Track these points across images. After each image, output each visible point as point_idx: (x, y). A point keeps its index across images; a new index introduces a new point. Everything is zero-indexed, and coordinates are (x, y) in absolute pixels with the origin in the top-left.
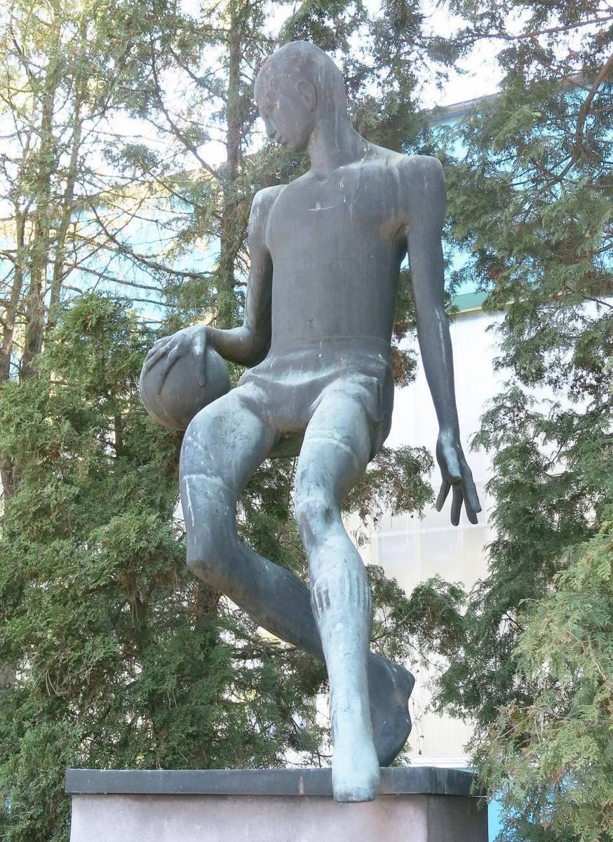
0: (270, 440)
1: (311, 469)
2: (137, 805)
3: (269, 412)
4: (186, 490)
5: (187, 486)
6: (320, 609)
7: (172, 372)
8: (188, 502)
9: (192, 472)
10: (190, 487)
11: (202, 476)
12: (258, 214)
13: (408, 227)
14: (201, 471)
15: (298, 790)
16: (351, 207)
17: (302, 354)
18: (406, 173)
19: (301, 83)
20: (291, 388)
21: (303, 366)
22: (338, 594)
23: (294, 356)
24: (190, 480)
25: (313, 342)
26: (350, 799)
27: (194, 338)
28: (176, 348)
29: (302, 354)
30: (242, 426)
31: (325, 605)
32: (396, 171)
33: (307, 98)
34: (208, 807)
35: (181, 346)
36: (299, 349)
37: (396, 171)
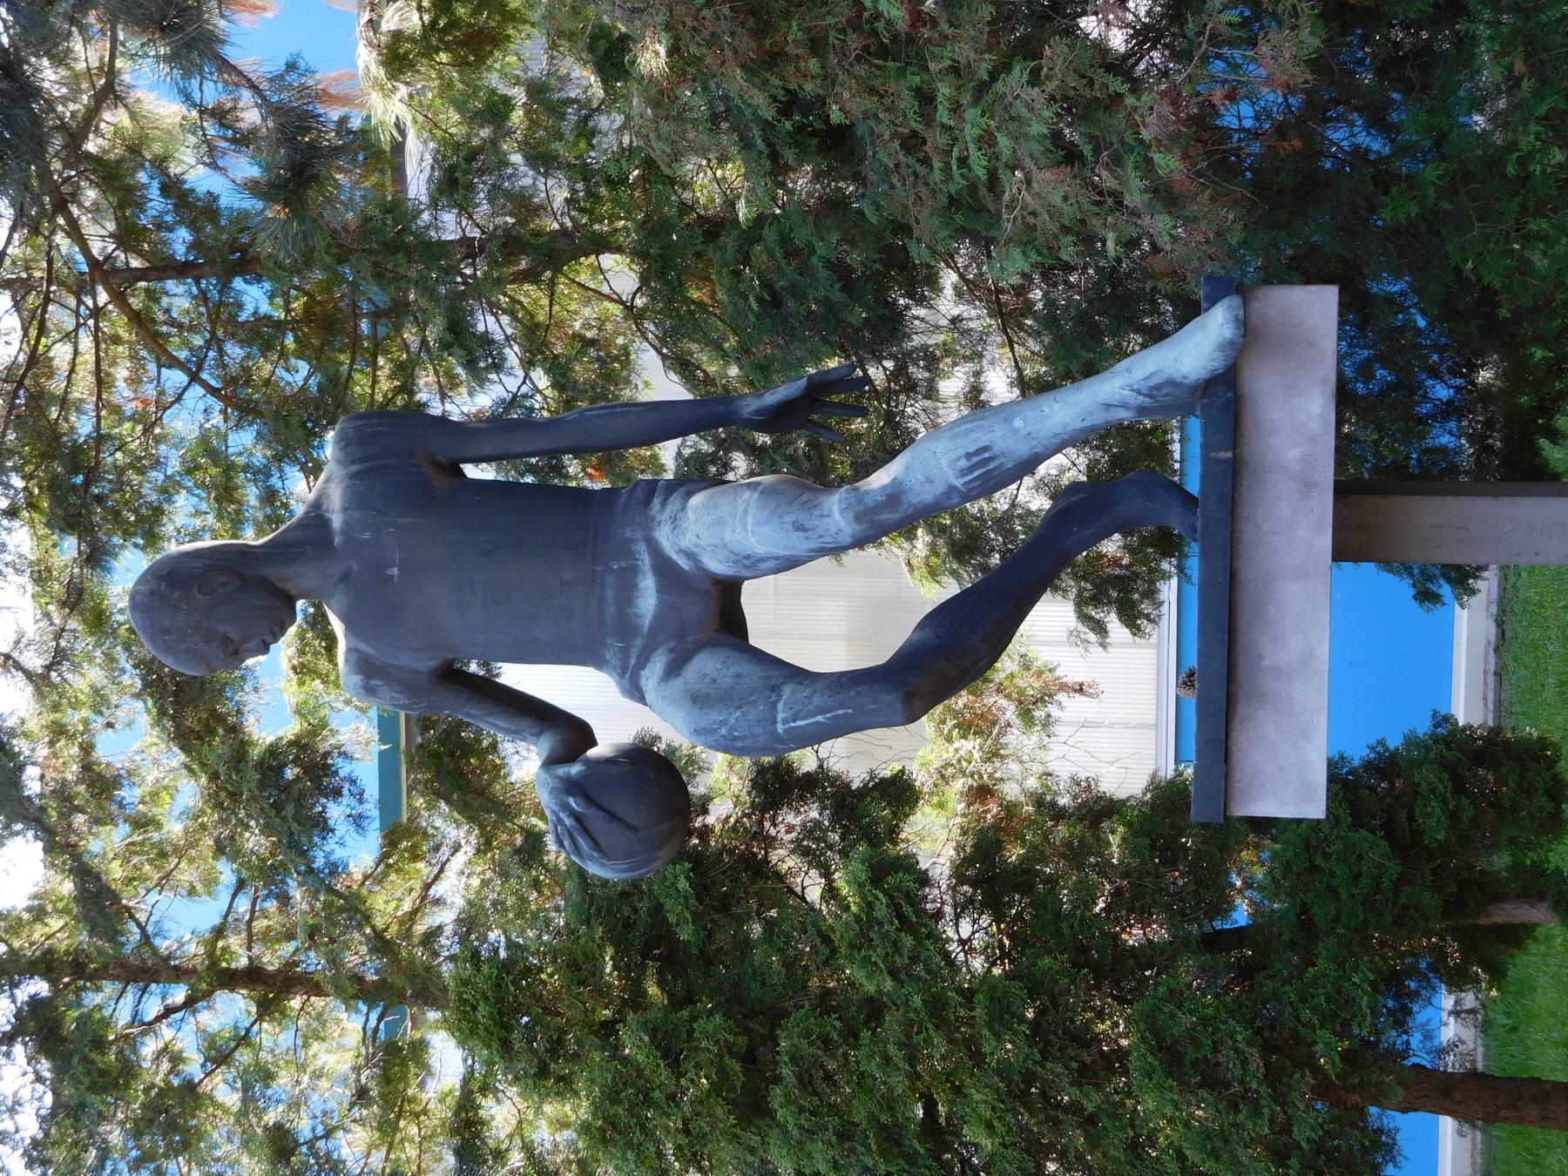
0: (732, 640)
1: (792, 518)
2: (1241, 709)
3: (690, 639)
4: (799, 727)
5: (792, 725)
6: (992, 465)
7: (606, 806)
8: (816, 723)
9: (774, 722)
10: (794, 721)
11: (780, 706)
12: (380, 683)
13: (439, 458)
14: (773, 708)
15: (1226, 460)
16: (401, 521)
17: (610, 595)
18: (359, 456)
19: (199, 589)
20: (661, 603)
21: (628, 591)
22: (974, 436)
23: (611, 610)
24: (785, 722)
25: (594, 581)
26: (1241, 317)
27: (558, 777)
28: (571, 801)
29: (610, 595)
30: (707, 671)
31: (987, 455)
32: (354, 468)
33: (224, 584)
34: (1245, 598)
35: (569, 792)
36: (601, 600)
37: (354, 468)
